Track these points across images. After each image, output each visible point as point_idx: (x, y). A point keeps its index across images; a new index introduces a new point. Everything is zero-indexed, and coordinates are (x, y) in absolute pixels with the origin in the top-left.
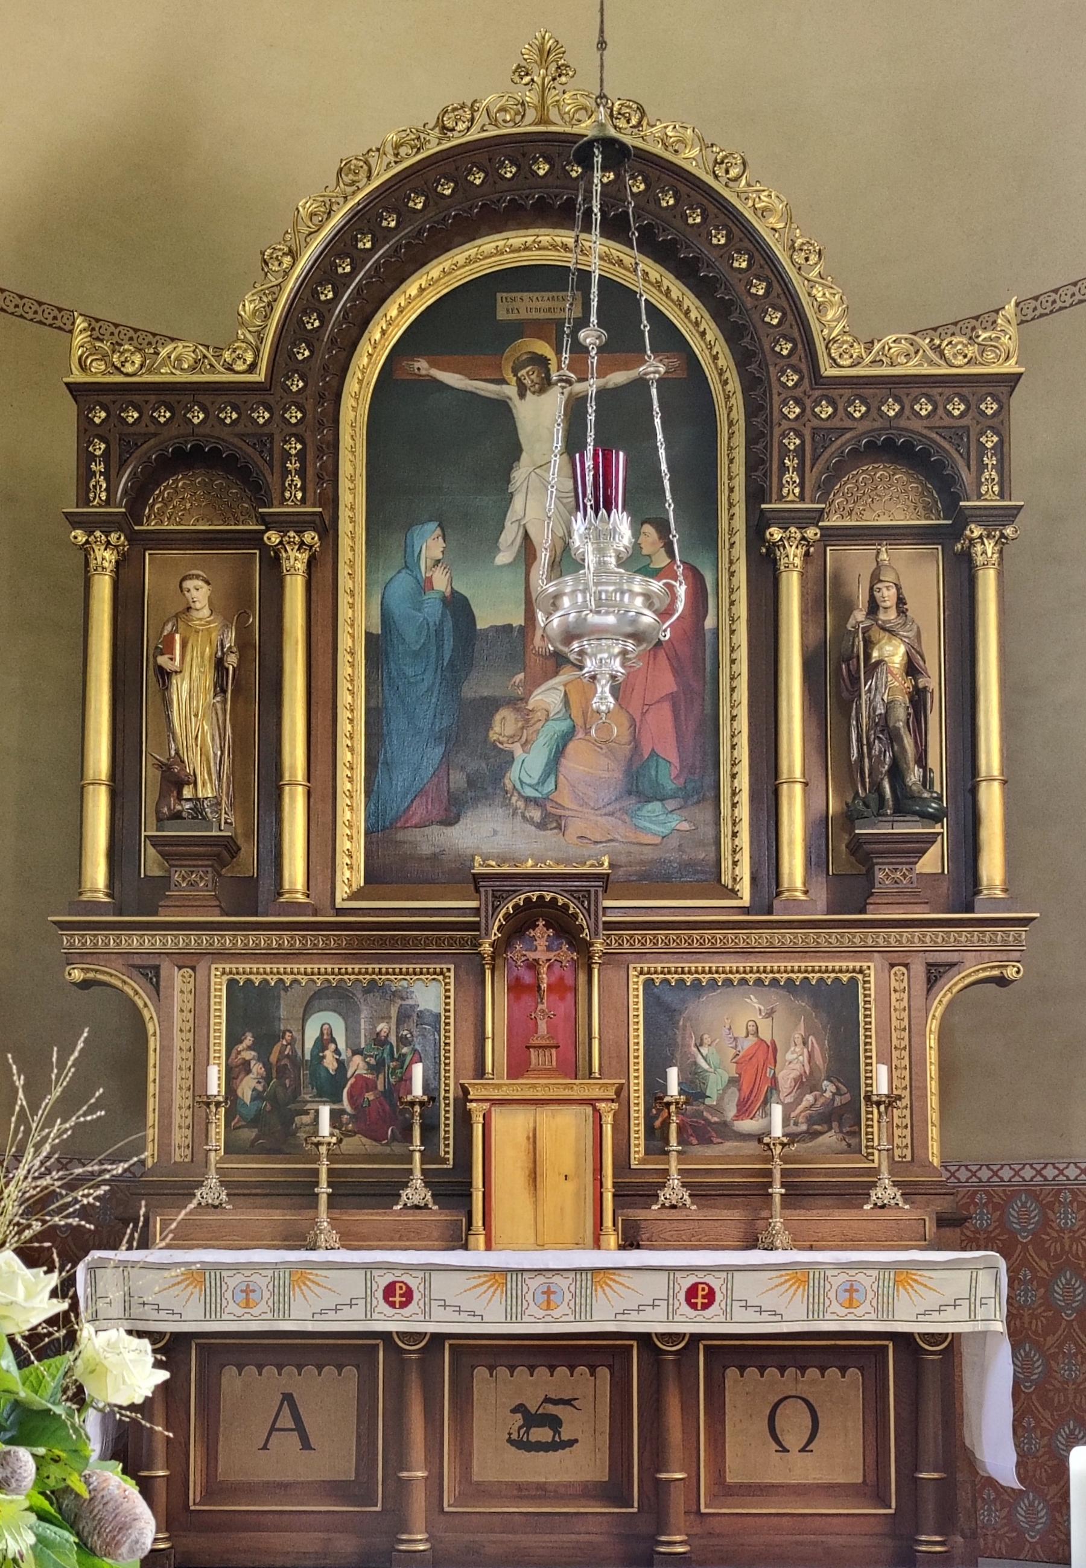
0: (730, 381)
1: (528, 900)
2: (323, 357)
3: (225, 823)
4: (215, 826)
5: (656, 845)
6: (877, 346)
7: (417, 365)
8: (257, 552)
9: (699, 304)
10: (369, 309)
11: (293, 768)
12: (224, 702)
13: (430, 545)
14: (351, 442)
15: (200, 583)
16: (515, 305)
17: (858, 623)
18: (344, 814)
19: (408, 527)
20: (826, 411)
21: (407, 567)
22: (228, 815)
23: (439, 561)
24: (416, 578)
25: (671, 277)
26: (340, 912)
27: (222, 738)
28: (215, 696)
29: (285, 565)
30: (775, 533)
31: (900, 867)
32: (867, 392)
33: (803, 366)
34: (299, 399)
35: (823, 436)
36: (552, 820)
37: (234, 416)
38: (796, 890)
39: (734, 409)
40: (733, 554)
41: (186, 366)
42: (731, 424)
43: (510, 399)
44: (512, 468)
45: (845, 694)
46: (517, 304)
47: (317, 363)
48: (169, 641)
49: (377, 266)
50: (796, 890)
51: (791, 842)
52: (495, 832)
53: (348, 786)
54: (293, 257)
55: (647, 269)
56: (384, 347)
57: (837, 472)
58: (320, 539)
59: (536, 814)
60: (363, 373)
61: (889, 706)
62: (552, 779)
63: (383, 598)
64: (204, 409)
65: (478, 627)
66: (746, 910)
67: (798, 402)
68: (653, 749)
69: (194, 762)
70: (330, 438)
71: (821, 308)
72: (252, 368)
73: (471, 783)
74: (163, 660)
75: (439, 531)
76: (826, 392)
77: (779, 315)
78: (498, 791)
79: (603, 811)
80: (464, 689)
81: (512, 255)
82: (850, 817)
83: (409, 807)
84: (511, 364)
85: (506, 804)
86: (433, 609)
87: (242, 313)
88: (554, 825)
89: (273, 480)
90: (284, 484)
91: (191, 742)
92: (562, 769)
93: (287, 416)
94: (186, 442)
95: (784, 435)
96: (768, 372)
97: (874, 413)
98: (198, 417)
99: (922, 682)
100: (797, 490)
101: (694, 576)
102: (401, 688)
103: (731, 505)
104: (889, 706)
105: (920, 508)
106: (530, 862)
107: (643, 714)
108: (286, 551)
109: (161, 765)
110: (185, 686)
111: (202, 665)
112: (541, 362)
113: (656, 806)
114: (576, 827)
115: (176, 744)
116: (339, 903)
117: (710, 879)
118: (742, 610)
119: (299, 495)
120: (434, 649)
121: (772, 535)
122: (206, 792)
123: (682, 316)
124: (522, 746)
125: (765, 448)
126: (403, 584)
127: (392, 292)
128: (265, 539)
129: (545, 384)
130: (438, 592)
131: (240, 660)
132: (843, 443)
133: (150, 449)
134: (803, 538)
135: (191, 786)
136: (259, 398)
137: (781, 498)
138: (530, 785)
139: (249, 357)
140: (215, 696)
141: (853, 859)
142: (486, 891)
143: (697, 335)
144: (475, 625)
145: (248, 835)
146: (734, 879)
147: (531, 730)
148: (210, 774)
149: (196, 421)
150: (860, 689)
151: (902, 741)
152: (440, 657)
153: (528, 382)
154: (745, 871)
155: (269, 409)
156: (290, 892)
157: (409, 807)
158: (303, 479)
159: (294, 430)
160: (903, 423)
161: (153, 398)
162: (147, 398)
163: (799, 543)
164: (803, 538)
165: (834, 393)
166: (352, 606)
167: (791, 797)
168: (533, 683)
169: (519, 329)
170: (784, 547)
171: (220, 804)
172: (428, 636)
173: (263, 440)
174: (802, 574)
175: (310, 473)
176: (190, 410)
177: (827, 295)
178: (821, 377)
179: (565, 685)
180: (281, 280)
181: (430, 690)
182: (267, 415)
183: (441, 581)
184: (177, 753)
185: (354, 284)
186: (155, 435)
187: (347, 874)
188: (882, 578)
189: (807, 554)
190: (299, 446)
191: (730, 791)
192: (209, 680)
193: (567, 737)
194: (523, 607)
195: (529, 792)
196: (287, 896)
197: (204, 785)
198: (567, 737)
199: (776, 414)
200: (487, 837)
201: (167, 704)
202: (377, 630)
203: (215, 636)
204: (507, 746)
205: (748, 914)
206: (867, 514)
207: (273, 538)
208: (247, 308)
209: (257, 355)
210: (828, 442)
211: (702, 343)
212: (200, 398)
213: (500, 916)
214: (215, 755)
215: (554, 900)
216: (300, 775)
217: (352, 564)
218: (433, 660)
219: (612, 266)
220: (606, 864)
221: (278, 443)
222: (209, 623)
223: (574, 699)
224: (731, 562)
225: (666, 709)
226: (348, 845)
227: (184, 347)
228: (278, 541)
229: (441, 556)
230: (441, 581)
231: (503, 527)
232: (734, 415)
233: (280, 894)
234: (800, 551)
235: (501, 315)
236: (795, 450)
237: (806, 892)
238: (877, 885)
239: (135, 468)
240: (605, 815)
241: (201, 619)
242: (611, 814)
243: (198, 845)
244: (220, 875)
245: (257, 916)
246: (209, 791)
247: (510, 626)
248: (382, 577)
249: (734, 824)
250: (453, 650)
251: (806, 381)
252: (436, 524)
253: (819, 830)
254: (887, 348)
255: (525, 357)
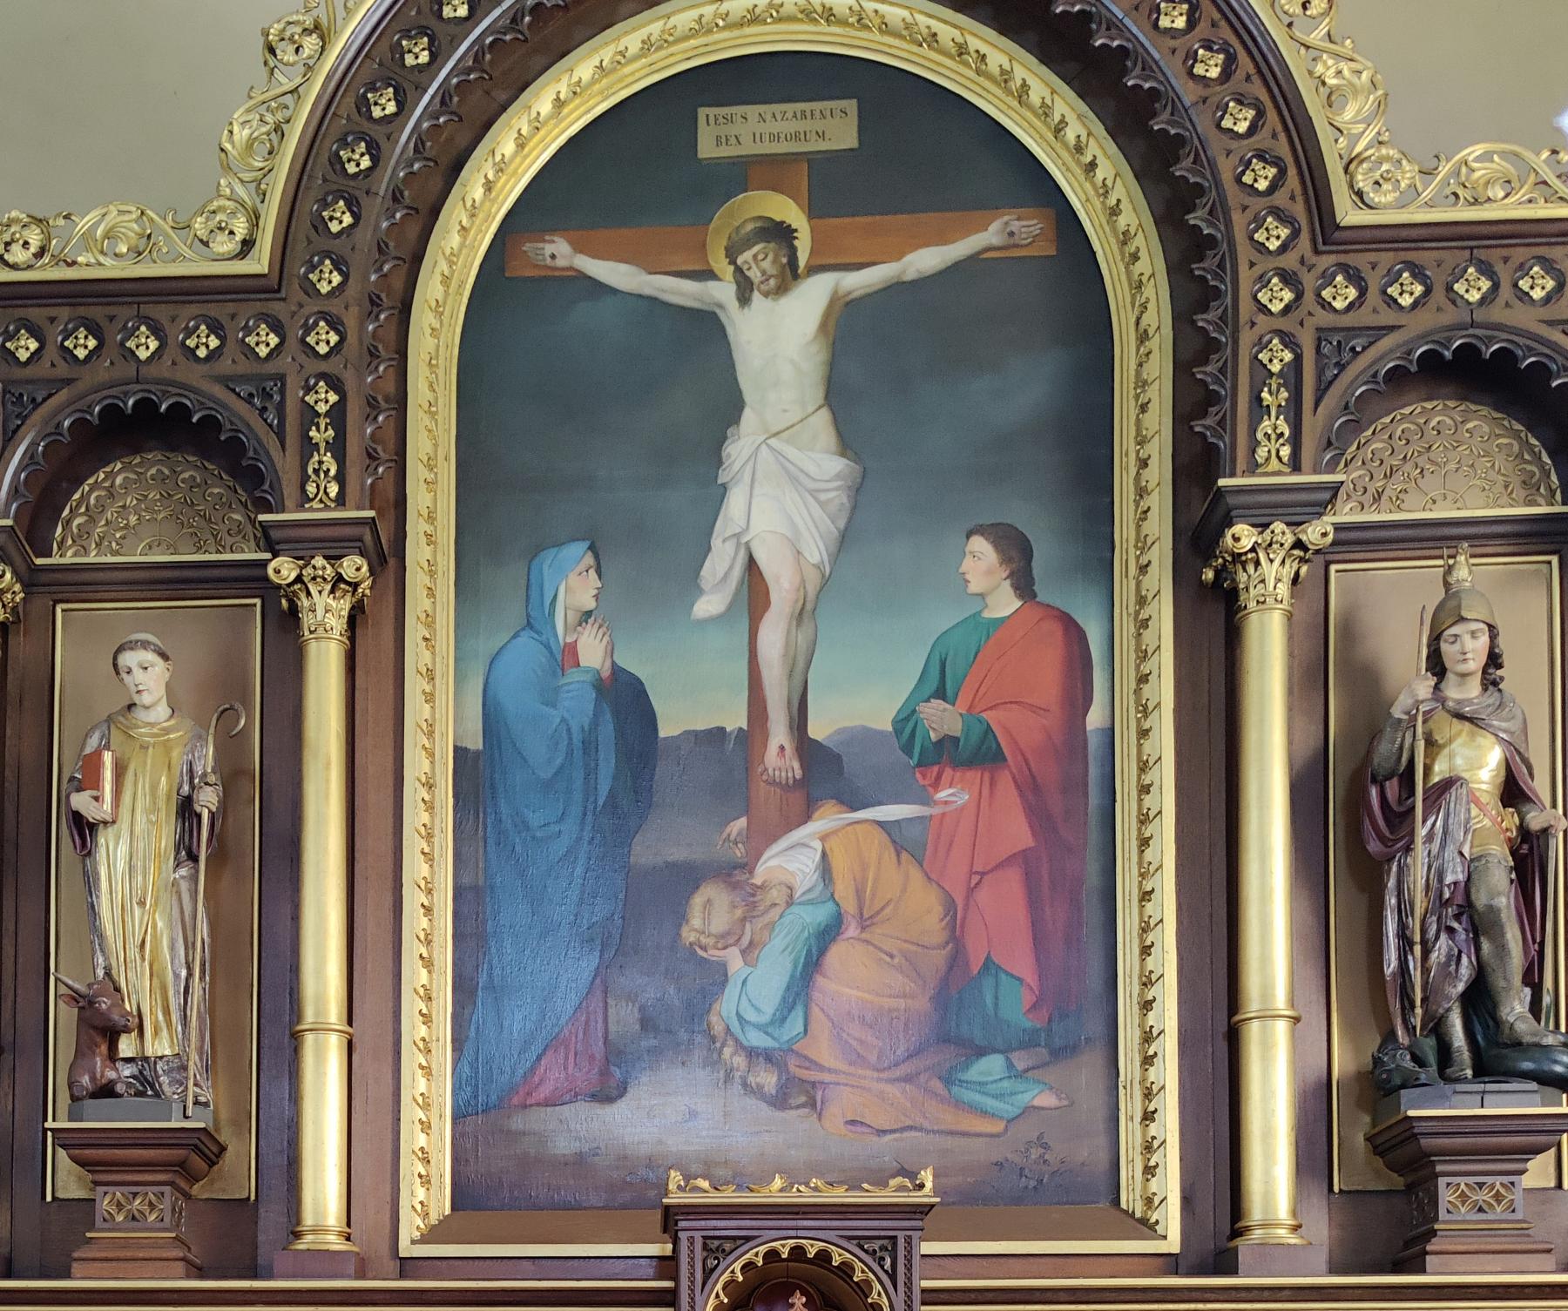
0: (1143, 254)
1: (772, 1255)
2: (377, 226)
3: (192, 1104)
4: (177, 1109)
5: (998, 1136)
6: (1445, 169)
7: (549, 249)
8: (258, 601)
9: (1083, 107)
10: (462, 141)
11: (321, 999)
12: (194, 878)
13: (574, 585)
14: (430, 396)
15: (149, 656)
16: (732, 130)
17: (1417, 704)
18: (414, 1084)
19: (535, 552)
20: (1342, 295)
21: (529, 625)
22: (200, 1087)
23: (589, 614)
24: (548, 647)
25: (1032, 60)
26: (407, 1267)
27: (189, 946)
28: (178, 866)
29: (307, 620)
30: (1243, 535)
31: (1489, 1180)
32: (1424, 257)
33: (1299, 210)
34: (335, 307)
35: (1338, 344)
36: (799, 1092)
37: (214, 342)
38: (1277, 1226)
39: (1152, 306)
40: (1145, 585)
41: (123, 248)
42: (1143, 337)
43: (721, 306)
44: (725, 438)
45: (1374, 846)
46: (737, 128)
47: (364, 237)
48: (92, 765)
49: (478, 51)
50: (1277, 1226)
51: (1268, 1134)
52: (693, 1114)
53: (423, 1031)
54: (322, 38)
55: (984, 49)
56: (489, 218)
57: (1357, 417)
58: (372, 571)
59: (768, 1080)
60: (451, 264)
61: (1473, 867)
62: (798, 1013)
63: (485, 691)
64: (156, 331)
65: (662, 734)
66: (1171, 1263)
67: (1288, 279)
68: (988, 958)
69: (139, 992)
70: (390, 387)
71: (1332, 99)
72: (248, 245)
73: (647, 1024)
74: (81, 801)
75: (589, 559)
76: (1342, 258)
77: (1251, 113)
78: (698, 1038)
79: (898, 1072)
80: (637, 848)
81: (726, 34)
82: (1379, 1086)
83: (533, 1069)
84: (724, 243)
85: (713, 1059)
86: (577, 703)
87: (228, 146)
88: (803, 1099)
89: (285, 463)
90: (304, 468)
91: (133, 952)
92: (816, 995)
93: (311, 340)
94: (127, 394)
95: (1262, 345)
96: (1229, 223)
97: (1439, 295)
98: (145, 346)
99: (1535, 821)
100: (1286, 452)
101: (1066, 630)
102: (518, 849)
103: (1142, 492)
104: (1473, 867)
105: (1515, 482)
106: (778, 1183)
107: (971, 891)
108: (309, 594)
109: (75, 997)
110: (123, 850)
111: (154, 808)
112: (781, 233)
113: (992, 1065)
114: (842, 1103)
115: (106, 959)
116: (406, 1249)
117: (1097, 1197)
118: (1164, 690)
119: (333, 490)
120: (578, 776)
121: (1236, 539)
122: (160, 1046)
123: (1050, 136)
124: (743, 952)
125: (1222, 370)
126: (525, 654)
127: (504, 108)
128: (270, 571)
129: (790, 275)
130: (588, 670)
131: (224, 803)
132: (1384, 354)
133: (59, 410)
134: (1299, 544)
135: (134, 1034)
136: (259, 307)
137: (1253, 467)
138: (758, 1027)
139: (241, 227)
140: (178, 866)
141: (1379, 1162)
142: (691, 1240)
143: (1078, 171)
144: (655, 729)
145: (240, 1124)
146: (1149, 1201)
147: (760, 922)
148: (167, 1012)
149: (143, 354)
150: (1412, 833)
151: (1503, 935)
152: (590, 789)
153: (754, 274)
154: (1170, 1183)
155: (277, 327)
156: (315, 1231)
157: (533, 1069)
158: (340, 459)
159: (324, 367)
160: (1497, 314)
161: (64, 313)
162: (53, 312)
163: (1288, 555)
164: (1299, 544)
165: (1359, 260)
166: (430, 698)
167: (1267, 1046)
168: (764, 836)
169: (742, 174)
170: (1257, 563)
171: (185, 1068)
172: (570, 753)
173: (266, 388)
174: (1290, 616)
175: (354, 449)
176: (131, 333)
177: (1346, 72)
178: (1338, 227)
179: (823, 839)
180: (298, 80)
181: (571, 851)
182: (274, 340)
183: (592, 652)
184: (108, 974)
185: (435, 85)
186: (68, 382)
187: (421, 1193)
188: (1465, 614)
189: (1295, 580)
190: (333, 398)
191: (1138, 1033)
192: (166, 835)
193: (828, 934)
194: (746, 694)
195: (756, 1039)
196: (310, 1238)
197: (156, 1032)
198: (828, 934)
199: (1246, 308)
200: (678, 1121)
201: (90, 883)
202: (475, 742)
203: (178, 756)
204: (714, 954)
205: (1176, 1272)
206: (1410, 499)
207: (283, 569)
208: (236, 137)
209: (255, 219)
210: (1347, 356)
211: (1088, 185)
212: (147, 310)
213: (719, 1286)
214: (177, 976)
215: (823, 1256)
216: (334, 1011)
217: (429, 620)
218: (578, 796)
219: (915, 49)
220: (929, 1185)
221: (294, 392)
222: (167, 731)
223: (839, 864)
224: (1142, 601)
225: (1012, 883)
226: (422, 1140)
227: (121, 212)
228: (293, 576)
229: (592, 604)
230: (592, 652)
231: (709, 549)
232: (1150, 319)
233: (297, 1235)
234: (1288, 571)
235: (707, 149)
236: (1281, 374)
237: (1296, 1228)
238: (1442, 1214)
239: (34, 444)
240: (898, 1080)
241: (152, 725)
242: (908, 1079)
243: (144, 1146)
244: (187, 1196)
245: (255, 1277)
246: (166, 1044)
247: (722, 730)
248: (486, 645)
249: (1148, 1095)
250: (615, 778)
251: (1305, 236)
252: (586, 544)
253: (1316, 1109)
254: (1464, 170)
255: (750, 227)
